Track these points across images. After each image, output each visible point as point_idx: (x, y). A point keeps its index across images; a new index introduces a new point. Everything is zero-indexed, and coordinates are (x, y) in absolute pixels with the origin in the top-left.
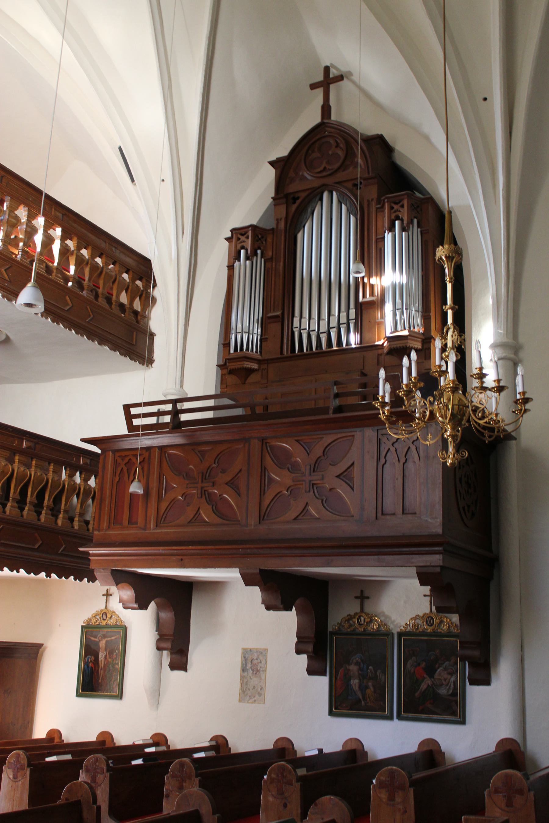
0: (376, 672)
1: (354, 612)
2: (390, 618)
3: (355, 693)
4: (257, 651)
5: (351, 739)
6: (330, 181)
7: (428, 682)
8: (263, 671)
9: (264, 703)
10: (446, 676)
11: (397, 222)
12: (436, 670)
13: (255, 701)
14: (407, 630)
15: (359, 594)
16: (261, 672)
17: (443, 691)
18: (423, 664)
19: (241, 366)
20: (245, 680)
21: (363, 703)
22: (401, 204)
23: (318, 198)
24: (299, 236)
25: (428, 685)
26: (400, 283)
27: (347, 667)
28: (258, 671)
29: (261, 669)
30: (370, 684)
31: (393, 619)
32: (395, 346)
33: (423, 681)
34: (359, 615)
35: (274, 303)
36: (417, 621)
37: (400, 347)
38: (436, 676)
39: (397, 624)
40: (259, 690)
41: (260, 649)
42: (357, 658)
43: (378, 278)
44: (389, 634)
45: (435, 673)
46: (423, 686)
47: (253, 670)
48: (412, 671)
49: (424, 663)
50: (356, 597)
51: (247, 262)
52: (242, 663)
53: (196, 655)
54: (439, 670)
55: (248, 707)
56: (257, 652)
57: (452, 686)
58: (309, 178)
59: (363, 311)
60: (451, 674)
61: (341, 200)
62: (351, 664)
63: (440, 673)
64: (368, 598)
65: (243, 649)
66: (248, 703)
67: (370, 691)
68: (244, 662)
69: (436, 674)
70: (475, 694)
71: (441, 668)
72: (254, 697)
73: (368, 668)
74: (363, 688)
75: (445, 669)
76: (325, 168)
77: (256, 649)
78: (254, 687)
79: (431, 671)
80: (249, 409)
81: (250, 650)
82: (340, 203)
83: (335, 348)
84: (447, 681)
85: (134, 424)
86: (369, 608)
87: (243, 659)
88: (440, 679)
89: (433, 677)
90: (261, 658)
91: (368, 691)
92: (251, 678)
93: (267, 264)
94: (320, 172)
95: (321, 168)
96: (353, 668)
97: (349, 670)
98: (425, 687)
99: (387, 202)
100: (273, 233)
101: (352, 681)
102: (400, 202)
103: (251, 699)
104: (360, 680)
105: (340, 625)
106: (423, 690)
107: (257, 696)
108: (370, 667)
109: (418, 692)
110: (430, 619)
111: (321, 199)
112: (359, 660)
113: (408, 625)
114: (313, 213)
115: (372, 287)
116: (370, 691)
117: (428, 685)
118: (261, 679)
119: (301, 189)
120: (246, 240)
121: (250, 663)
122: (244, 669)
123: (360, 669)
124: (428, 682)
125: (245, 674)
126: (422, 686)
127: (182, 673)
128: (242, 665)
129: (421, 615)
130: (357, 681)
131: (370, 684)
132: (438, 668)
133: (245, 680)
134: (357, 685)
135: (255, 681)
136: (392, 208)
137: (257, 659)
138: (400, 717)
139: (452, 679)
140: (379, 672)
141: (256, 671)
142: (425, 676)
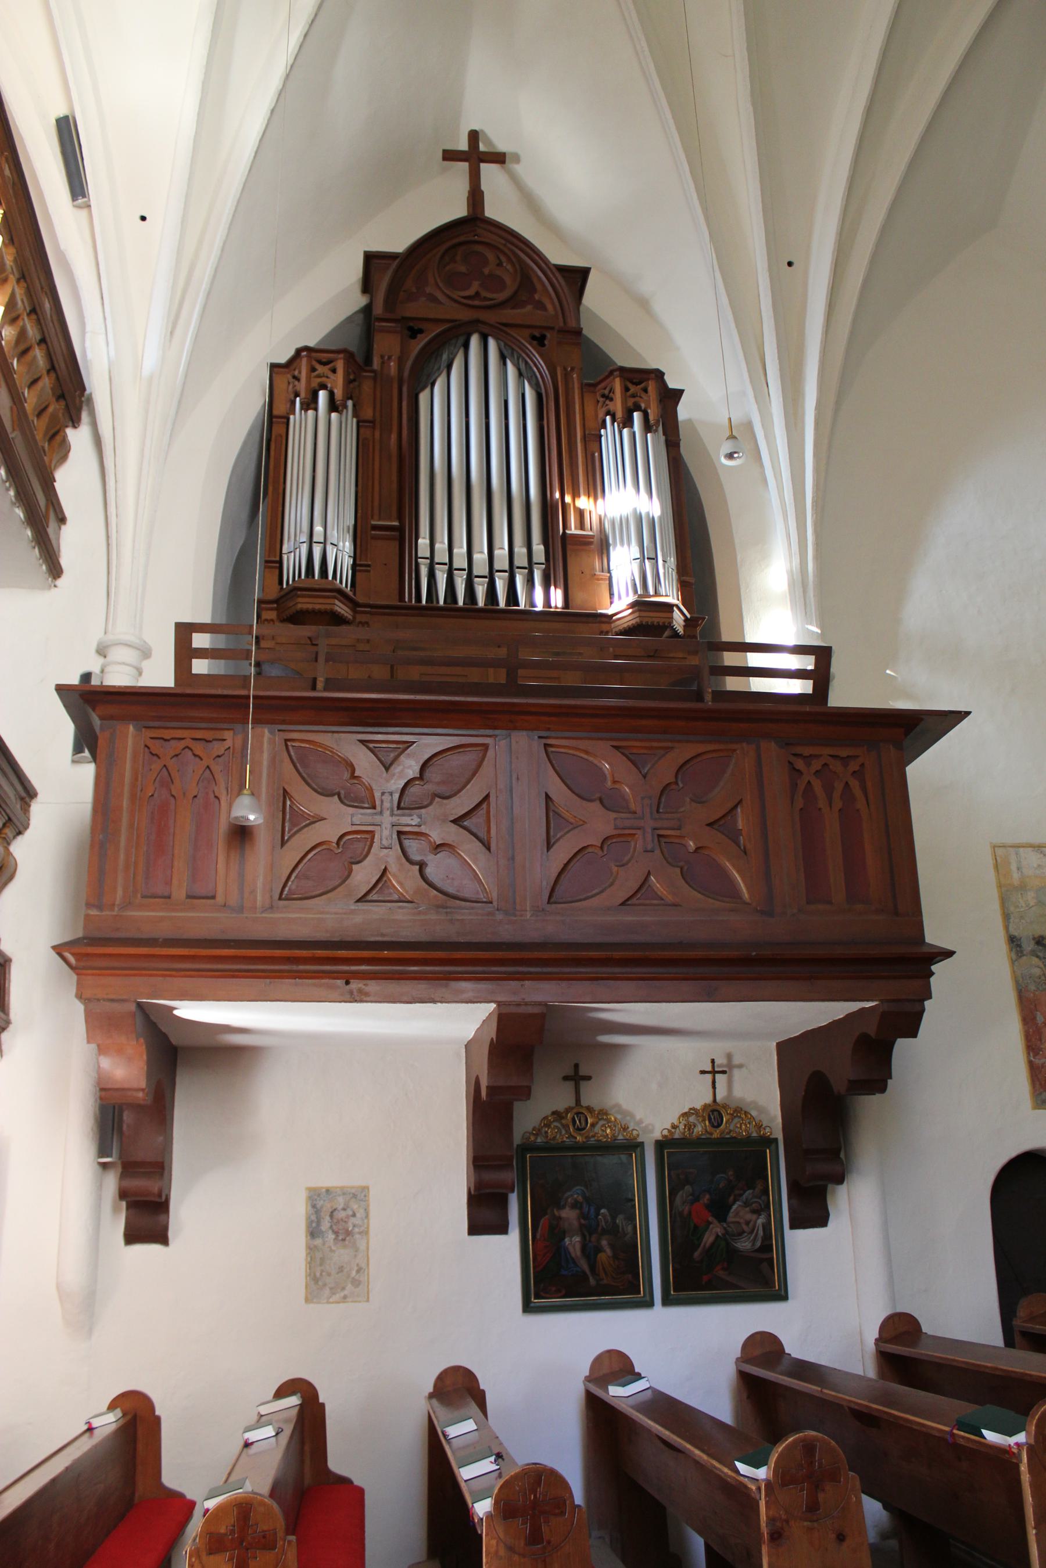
0: (614, 1218)
1: (566, 1105)
2: (632, 1116)
3: (574, 1262)
4: (344, 1191)
5: (609, 1352)
6: (491, 317)
7: (716, 1229)
8: (360, 1233)
9: (368, 1300)
10: (749, 1216)
11: (635, 414)
12: (730, 1207)
13: (345, 1297)
14: (676, 1136)
15: (570, 1072)
16: (357, 1236)
17: (744, 1245)
18: (706, 1199)
19: (328, 607)
20: (319, 1255)
21: (592, 1281)
22: (643, 385)
23: (461, 340)
24: (423, 397)
25: (717, 1236)
26: (648, 513)
27: (556, 1213)
28: (348, 1233)
29: (356, 1230)
30: (604, 1243)
31: (638, 1117)
32: (650, 621)
33: (706, 1230)
34: (575, 1111)
35: (380, 506)
36: (692, 1119)
37: (653, 623)
38: (731, 1217)
39: (647, 1126)
40: (354, 1273)
41: (353, 1187)
42: (576, 1193)
43: (592, 500)
44: (634, 1146)
45: (728, 1211)
46: (708, 1239)
47: (336, 1233)
48: (686, 1212)
49: (707, 1196)
50: (566, 1078)
51: (334, 415)
52: (308, 1218)
53: (186, 1211)
54: (735, 1207)
55: (329, 1313)
56: (344, 1194)
57: (761, 1233)
58: (437, 304)
59: (569, 553)
60: (757, 1212)
61: (505, 353)
62: (564, 1207)
63: (738, 1212)
64: (588, 1078)
65: (310, 1190)
66: (328, 1302)
67: (605, 1256)
68: (313, 1218)
69: (731, 1214)
70: (802, 1246)
71: (738, 1203)
72: (343, 1289)
73: (598, 1214)
74: (590, 1252)
75: (746, 1204)
76: (477, 294)
77: (342, 1188)
78: (341, 1269)
79: (720, 1210)
80: (503, 672)
81: (328, 1191)
82: (503, 358)
83: (522, 606)
84: (751, 1225)
85: (194, 671)
86: (591, 1097)
87: (311, 1211)
88: (738, 1223)
89: (725, 1220)
90: (355, 1207)
91: (602, 1256)
92: (332, 1251)
93: (362, 431)
94: (465, 298)
95: (471, 292)
96: (569, 1215)
97: (560, 1218)
98: (712, 1239)
99: (620, 376)
100: (375, 379)
101: (567, 1241)
102: (640, 383)
103: (334, 1294)
104: (583, 1236)
105: (537, 1131)
106: (708, 1245)
107: (349, 1287)
108: (603, 1211)
109: (700, 1250)
110: (716, 1113)
111: (466, 346)
112: (580, 1199)
113: (674, 1127)
114: (449, 367)
115: (581, 513)
116: (605, 1256)
117: (717, 1236)
118: (357, 1250)
119: (432, 316)
120: (330, 374)
121: (328, 1218)
122: (313, 1232)
123: (583, 1216)
124: (716, 1229)
125: (318, 1242)
126: (705, 1239)
127: (155, 1248)
128: (309, 1223)
129: (698, 1106)
130: (577, 1239)
131: (604, 1243)
132: (734, 1204)
133: (319, 1255)
134: (578, 1247)
135: (341, 1255)
136: (627, 389)
137: (344, 1209)
138: (668, 1301)
139: (761, 1221)
140: (620, 1220)
141: (344, 1234)
142: (710, 1219)
